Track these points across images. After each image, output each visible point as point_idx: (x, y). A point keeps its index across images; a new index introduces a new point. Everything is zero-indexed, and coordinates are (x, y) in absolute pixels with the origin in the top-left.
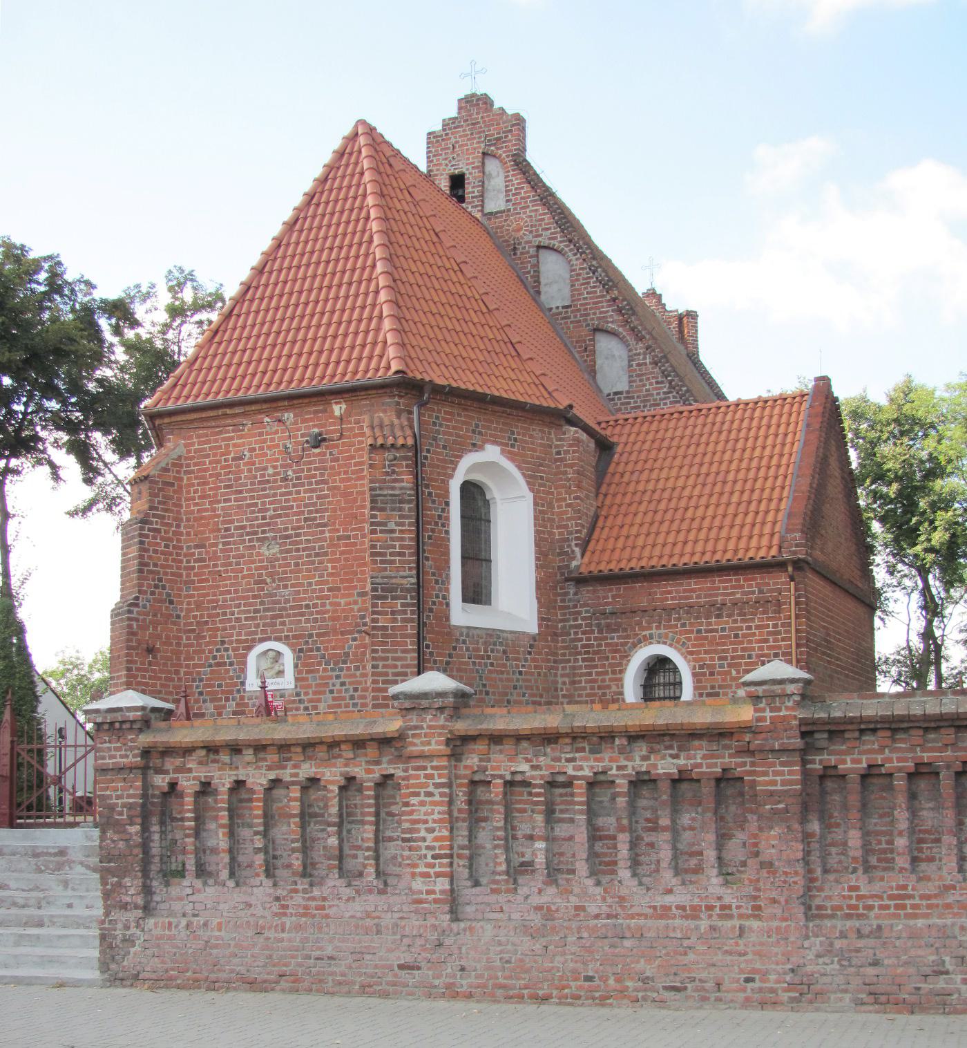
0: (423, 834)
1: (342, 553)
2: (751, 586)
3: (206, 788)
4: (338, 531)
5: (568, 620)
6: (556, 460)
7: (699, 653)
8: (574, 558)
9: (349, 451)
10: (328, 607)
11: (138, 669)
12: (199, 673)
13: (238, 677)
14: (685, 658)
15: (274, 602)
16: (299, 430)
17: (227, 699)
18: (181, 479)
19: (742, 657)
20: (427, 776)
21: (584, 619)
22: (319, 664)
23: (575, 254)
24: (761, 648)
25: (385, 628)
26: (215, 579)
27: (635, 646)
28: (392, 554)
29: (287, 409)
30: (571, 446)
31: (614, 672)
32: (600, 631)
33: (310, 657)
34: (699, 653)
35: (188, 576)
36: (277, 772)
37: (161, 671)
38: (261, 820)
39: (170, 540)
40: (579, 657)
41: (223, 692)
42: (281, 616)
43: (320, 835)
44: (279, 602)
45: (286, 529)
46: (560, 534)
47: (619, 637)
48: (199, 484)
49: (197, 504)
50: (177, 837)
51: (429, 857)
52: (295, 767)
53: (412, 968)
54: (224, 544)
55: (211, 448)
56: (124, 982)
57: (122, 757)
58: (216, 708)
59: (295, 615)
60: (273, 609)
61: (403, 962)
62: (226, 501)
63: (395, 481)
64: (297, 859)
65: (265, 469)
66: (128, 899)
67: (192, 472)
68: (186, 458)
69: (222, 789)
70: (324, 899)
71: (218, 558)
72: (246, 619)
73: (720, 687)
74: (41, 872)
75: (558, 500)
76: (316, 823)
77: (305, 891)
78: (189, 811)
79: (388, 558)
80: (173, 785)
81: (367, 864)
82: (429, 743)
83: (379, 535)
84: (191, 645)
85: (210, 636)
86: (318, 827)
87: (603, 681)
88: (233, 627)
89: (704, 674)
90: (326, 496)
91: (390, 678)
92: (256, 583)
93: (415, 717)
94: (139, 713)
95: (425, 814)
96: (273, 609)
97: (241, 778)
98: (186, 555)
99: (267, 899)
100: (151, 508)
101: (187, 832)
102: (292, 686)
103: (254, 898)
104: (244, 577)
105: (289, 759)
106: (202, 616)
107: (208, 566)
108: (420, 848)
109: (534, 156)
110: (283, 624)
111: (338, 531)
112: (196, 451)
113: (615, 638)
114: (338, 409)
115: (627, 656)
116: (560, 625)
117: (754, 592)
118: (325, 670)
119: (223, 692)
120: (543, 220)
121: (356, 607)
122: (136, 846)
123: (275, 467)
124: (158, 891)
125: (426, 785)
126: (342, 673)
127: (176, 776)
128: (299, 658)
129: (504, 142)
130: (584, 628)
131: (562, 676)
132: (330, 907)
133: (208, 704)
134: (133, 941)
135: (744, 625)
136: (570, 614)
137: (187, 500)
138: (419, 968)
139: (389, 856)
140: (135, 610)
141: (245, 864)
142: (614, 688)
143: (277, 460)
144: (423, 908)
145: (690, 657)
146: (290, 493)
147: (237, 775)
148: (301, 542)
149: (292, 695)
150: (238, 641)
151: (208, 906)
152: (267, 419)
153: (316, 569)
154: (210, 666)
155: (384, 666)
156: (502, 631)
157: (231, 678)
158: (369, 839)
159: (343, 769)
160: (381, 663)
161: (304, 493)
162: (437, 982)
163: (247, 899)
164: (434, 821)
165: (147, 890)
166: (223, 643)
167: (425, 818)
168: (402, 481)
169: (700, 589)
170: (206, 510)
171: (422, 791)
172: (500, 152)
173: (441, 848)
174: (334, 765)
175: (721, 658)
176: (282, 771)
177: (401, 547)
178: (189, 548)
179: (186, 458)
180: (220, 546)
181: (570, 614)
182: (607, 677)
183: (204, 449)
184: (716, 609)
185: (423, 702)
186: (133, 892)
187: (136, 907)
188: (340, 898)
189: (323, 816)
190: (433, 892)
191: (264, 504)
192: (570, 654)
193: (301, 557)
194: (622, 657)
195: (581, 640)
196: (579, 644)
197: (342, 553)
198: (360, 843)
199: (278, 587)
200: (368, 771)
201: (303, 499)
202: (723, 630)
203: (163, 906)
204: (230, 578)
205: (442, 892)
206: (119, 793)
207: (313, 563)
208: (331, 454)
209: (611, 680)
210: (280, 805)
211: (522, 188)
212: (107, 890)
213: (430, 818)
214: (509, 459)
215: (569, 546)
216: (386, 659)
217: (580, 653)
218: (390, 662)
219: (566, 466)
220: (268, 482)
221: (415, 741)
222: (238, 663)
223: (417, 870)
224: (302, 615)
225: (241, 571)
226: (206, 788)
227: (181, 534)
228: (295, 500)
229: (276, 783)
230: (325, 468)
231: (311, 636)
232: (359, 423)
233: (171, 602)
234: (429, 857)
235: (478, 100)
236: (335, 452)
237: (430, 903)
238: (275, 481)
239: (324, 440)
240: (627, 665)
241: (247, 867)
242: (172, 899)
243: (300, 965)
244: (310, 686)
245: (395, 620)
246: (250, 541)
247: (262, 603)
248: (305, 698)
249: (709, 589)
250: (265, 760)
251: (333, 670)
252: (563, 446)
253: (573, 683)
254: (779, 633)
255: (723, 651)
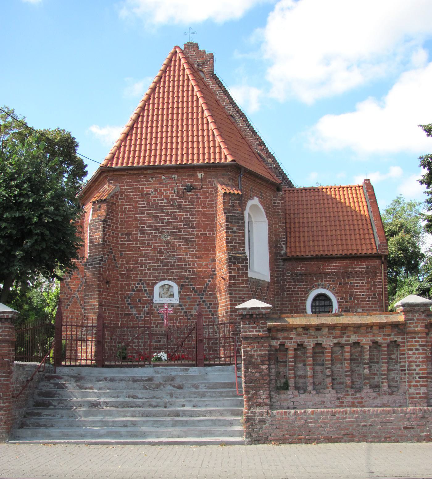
0: (414, 367)
1: (203, 241)
2: (363, 265)
3: (301, 346)
4: (201, 231)
5: (280, 277)
6: (274, 206)
7: (340, 293)
8: (282, 250)
9: (206, 195)
10: (196, 266)
11: (103, 291)
12: (128, 294)
13: (149, 297)
14: (334, 295)
15: (168, 262)
16: (180, 183)
17: (143, 307)
18: (118, 202)
19: (360, 295)
20: (416, 342)
21: (287, 276)
22: (192, 292)
23: (239, 118)
24: (368, 292)
25: (235, 276)
26: (136, 250)
27: (311, 289)
28: (235, 243)
29: (174, 173)
30: (280, 200)
31: (301, 300)
32: (295, 282)
33: (187, 288)
34: (340, 293)
35: (122, 248)
36: (339, 339)
37: (111, 293)
38: (330, 362)
39: (114, 230)
40: (285, 293)
41: (141, 304)
42: (172, 269)
43: (356, 369)
44: (171, 262)
45: (174, 229)
46: (275, 239)
47: (304, 285)
48: (127, 205)
49: (126, 214)
50: (281, 370)
51: (417, 378)
52: (348, 337)
53: (411, 428)
54: (141, 234)
55: (133, 188)
56: (260, 442)
57: (256, 331)
58: (137, 311)
59: (179, 269)
60: (168, 266)
61: (405, 426)
62: (142, 214)
63: (234, 210)
64: (349, 380)
65: (163, 200)
66: (262, 401)
67: (124, 199)
68: (120, 192)
69: (310, 347)
70: (362, 398)
71: (138, 240)
72: (153, 270)
73: (350, 308)
74: (147, 389)
75: (275, 224)
76: (354, 363)
77: (352, 395)
78: (291, 358)
79: (234, 244)
80: (282, 345)
81: (384, 382)
82: (417, 327)
83: (230, 234)
84: (124, 281)
85: (134, 277)
86: (355, 365)
87: (297, 303)
88: (147, 273)
89: (343, 302)
90: (194, 215)
91: (237, 299)
92: (158, 253)
93: (410, 315)
94: (269, 310)
95: (416, 358)
96: (168, 266)
97: (319, 342)
98: (120, 238)
99: (333, 399)
100: (107, 215)
101: (290, 368)
102: (178, 302)
103: (326, 399)
104: (152, 250)
105: (345, 333)
106: (129, 267)
107: (133, 244)
108: (413, 374)
109: (218, 72)
110: (173, 272)
111: (201, 231)
112: (126, 189)
113: (302, 285)
114: (200, 175)
115: (307, 293)
116: (276, 279)
117: (364, 268)
118: (194, 295)
119: (141, 304)
120: (224, 101)
121: (210, 267)
122: (265, 375)
123: (168, 200)
124: (274, 397)
125: (415, 345)
126: (203, 296)
127: (284, 341)
128: (181, 289)
129: (206, 65)
130: (287, 281)
131: (277, 301)
132: (365, 402)
133: (133, 309)
134: (265, 422)
135: (361, 282)
136: (281, 274)
137: (121, 212)
138: (413, 428)
139: (391, 378)
140: (102, 263)
141: (318, 383)
142: (302, 307)
143: (169, 196)
144: (414, 401)
145: (336, 295)
146: (176, 212)
147: (317, 341)
148: (181, 235)
149: (178, 306)
150: (149, 280)
151: (301, 403)
152: (163, 177)
153: (189, 248)
154: (134, 291)
155: (235, 294)
156: (260, 280)
157: (145, 297)
158: (385, 370)
159: (372, 338)
160: (233, 292)
161: (183, 212)
162: (422, 434)
163: (323, 399)
164: (420, 362)
165: (270, 397)
166: (141, 280)
167: (415, 360)
168: (237, 210)
169: (341, 266)
170: (132, 217)
171: (414, 348)
172: (204, 69)
173: (423, 373)
174: (368, 336)
175: (350, 295)
176: (341, 339)
177: (239, 240)
178: (122, 234)
179: (120, 192)
180: (139, 235)
181: (281, 274)
182: (298, 302)
183: (131, 189)
184: (346, 274)
185: (416, 308)
186: (264, 397)
187: (266, 405)
188: (370, 398)
189: (357, 360)
190: (419, 393)
191: (162, 216)
192: (281, 292)
193: (182, 242)
194: (305, 294)
195: (286, 285)
196: (285, 287)
197: (203, 241)
198: (376, 372)
199: (170, 255)
200: (384, 339)
201: (183, 215)
202: (351, 283)
203: (276, 404)
204: (144, 250)
205: (423, 393)
206: (256, 349)
207: (188, 245)
208: (197, 195)
209: (300, 303)
210: (336, 355)
211: (215, 86)
212: (249, 397)
213: (418, 360)
214: (261, 204)
215: (280, 244)
216: (235, 290)
217: (285, 291)
218: (237, 292)
219: (278, 209)
220: (164, 206)
221: (411, 325)
222: (149, 290)
223: (412, 384)
224: (183, 269)
225: (151, 247)
226: (301, 346)
227: (118, 228)
228: (178, 215)
229: (337, 344)
230: (193, 202)
231: (187, 279)
232: (211, 182)
233: (115, 260)
234: (417, 378)
235: (193, 45)
236: (199, 194)
237: (418, 398)
238: (168, 206)
239: (193, 189)
240: (307, 297)
241: (319, 384)
242: (281, 400)
243: (354, 429)
244: (187, 302)
245: (239, 273)
246: (155, 233)
247: (162, 262)
248: (185, 307)
249: (345, 266)
250: (332, 333)
251: (198, 295)
252: (276, 200)
253: (283, 304)
254: (376, 285)
255: (351, 292)
